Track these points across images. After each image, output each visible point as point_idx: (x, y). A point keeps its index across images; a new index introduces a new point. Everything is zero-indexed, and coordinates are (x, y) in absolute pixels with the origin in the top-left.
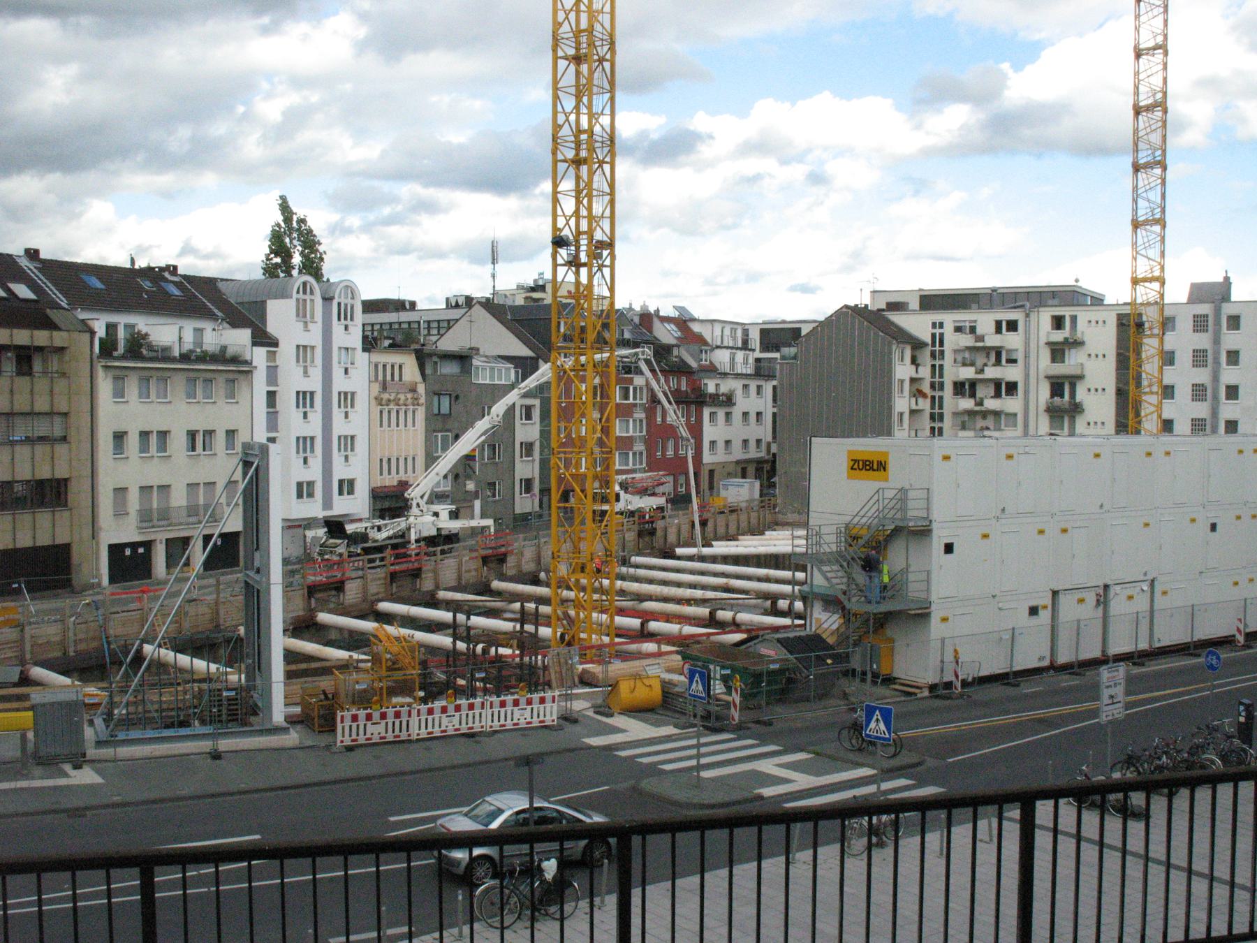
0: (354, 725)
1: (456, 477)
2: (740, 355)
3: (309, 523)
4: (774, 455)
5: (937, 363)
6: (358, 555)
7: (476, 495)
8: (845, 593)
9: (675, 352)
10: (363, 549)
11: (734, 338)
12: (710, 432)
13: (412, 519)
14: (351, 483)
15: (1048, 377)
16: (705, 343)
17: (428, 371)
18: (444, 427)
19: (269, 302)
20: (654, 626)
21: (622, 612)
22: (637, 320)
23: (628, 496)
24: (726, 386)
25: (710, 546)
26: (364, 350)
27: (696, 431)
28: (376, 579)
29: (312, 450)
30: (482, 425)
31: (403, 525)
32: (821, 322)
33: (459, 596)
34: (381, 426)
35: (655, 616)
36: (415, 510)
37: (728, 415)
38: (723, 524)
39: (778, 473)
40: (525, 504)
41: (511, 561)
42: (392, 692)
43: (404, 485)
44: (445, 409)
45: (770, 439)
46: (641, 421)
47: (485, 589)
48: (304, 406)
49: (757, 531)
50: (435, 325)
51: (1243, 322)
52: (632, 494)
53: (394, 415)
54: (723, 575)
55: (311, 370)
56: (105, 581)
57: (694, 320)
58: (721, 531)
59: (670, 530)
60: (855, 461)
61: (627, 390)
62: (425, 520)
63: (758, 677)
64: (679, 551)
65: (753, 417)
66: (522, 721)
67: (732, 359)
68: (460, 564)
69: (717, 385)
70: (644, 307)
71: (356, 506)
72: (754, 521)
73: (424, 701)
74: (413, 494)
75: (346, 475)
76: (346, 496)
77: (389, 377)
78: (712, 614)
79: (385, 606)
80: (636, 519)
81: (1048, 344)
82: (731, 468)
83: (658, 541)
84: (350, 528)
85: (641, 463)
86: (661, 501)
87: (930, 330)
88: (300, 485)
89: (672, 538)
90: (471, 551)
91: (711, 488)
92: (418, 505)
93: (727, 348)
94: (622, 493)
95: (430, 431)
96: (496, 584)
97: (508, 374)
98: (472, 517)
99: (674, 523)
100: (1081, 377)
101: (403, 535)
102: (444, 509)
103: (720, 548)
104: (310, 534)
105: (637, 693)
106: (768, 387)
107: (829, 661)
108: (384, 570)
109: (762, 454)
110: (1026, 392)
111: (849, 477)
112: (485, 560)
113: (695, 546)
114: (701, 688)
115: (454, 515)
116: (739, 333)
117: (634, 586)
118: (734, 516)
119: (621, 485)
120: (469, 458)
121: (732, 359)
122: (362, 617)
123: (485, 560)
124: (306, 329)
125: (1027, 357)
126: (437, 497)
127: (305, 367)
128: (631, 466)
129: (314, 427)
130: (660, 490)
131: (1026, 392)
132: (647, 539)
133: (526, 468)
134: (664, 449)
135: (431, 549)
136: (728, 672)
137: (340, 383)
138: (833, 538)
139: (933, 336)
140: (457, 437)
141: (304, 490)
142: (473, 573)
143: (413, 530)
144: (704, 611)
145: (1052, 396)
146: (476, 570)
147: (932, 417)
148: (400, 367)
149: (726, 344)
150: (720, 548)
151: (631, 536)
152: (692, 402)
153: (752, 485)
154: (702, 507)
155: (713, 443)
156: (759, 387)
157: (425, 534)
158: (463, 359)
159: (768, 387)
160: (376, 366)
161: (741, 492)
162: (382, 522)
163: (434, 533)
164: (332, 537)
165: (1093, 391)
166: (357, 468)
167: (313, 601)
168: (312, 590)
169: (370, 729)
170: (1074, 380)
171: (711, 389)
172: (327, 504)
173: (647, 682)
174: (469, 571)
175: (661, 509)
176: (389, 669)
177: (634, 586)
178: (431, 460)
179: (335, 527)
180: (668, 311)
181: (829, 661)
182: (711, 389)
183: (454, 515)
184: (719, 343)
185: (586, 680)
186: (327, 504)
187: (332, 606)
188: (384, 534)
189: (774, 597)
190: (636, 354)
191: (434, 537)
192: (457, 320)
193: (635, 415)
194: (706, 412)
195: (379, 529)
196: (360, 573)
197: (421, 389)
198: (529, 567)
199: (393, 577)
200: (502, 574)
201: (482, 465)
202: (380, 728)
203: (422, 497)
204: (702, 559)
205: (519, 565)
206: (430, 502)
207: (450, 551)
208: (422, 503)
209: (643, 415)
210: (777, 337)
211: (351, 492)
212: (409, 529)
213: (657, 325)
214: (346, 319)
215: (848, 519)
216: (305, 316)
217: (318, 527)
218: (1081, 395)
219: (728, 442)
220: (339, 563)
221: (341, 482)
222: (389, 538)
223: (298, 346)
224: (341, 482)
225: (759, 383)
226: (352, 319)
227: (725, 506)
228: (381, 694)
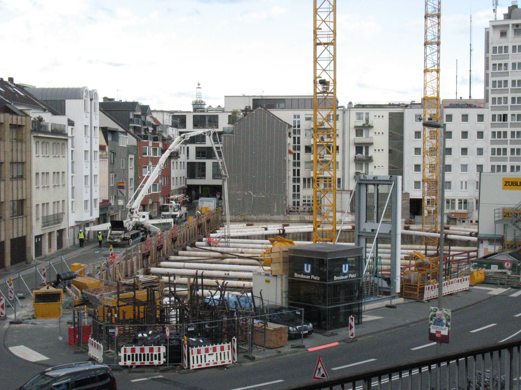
0: (222, 353)
5: (297, 136)
15: (355, 144)
19: (67, 101)
51: (453, 117)
56: (34, 257)
60: (507, 182)
66: (211, 362)
81: (355, 127)
87: (293, 119)
100: (372, 144)
110: (343, 151)
111: (503, 189)
125: (344, 133)
131: (343, 151)
139: (295, 122)
145: (356, 154)
147: (294, 164)
165: (377, 150)
169: (209, 358)
170: (368, 145)
202: (213, 357)
218: (371, 153)
219: (177, 178)
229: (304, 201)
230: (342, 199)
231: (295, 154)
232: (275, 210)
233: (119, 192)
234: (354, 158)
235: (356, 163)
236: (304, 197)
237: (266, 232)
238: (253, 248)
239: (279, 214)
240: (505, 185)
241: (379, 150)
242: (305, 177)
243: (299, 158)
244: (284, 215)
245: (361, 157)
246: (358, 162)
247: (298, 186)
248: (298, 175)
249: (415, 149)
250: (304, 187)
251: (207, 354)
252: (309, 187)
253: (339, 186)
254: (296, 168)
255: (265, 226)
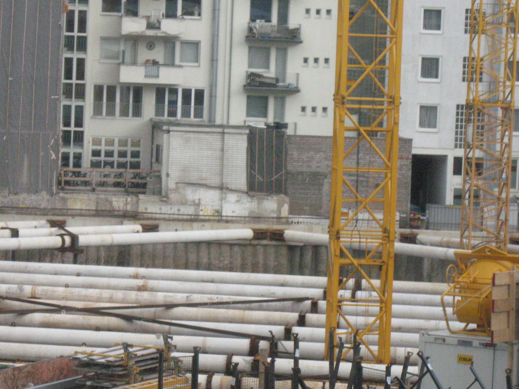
145: (253, 19)
229: (96, 153)
230: (222, 150)
231: (73, 12)
232: (24, 178)
234: (245, 33)
235: (250, 48)
236: (97, 141)
237: (12, 243)
238: (67, 286)
239: (36, 192)
241: (318, 12)
242: (99, 82)
243: (83, 27)
244: (52, 195)
245: (269, 30)
246: (258, 43)
247: (80, 110)
248: (81, 75)
249: (426, 11)
250: (97, 111)
252: (111, 112)
253: (199, 114)
254: (75, 56)
255: (13, 225)
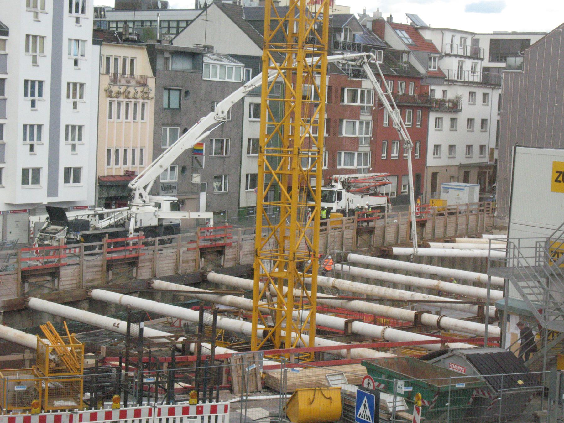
0: (213, 416)
1: (183, 169)
2: (468, 64)
3: (33, 209)
4: (496, 160)
6: (78, 242)
7: (202, 188)
8: (540, 311)
9: (405, 58)
10: (82, 236)
11: (464, 47)
12: (434, 137)
13: (134, 209)
14: (37, 171)
16: (435, 51)
17: (160, 65)
18: (173, 120)
20: (358, 326)
21: (324, 309)
22: (369, 26)
23: (349, 195)
24: (452, 93)
25: (428, 246)
26: (95, 43)
27: (420, 136)
28: (92, 265)
29: (39, 138)
30: (208, 120)
31: (125, 214)
32: (546, 34)
33: (174, 286)
34: (110, 117)
35: (361, 316)
36: (137, 200)
37: (453, 120)
38: (442, 225)
39: (498, 180)
40: (249, 198)
41: (229, 253)
42: (56, 393)
43: (130, 175)
44: (174, 104)
45: (493, 145)
46: (368, 123)
47: (200, 280)
48: (33, 94)
49: (475, 234)
50: (175, 24)
52: (354, 193)
53: (131, 107)
54: (433, 276)
55: (39, 60)
57: (426, 28)
58: (439, 232)
59: (388, 230)
61: (355, 92)
62: (146, 211)
63: (443, 395)
64: (397, 250)
65: (477, 124)
67: (460, 67)
68: (178, 254)
69: (444, 92)
70: (377, 13)
71: (81, 195)
72: (472, 224)
73: (92, 404)
74: (136, 184)
75: (73, 164)
76: (71, 184)
77: (120, 71)
78: (418, 316)
79: (99, 293)
80: (356, 217)
82: (454, 173)
83: (376, 240)
84: (71, 215)
85: (366, 164)
86: (381, 201)
88: (25, 172)
89: (390, 237)
90: (192, 242)
91: (434, 188)
92: (141, 195)
93: (456, 56)
94: (344, 192)
95: (159, 124)
96: (213, 276)
97: (238, 72)
98: (198, 210)
99: (391, 224)
101: (123, 224)
102: (166, 201)
103: (437, 249)
104: (34, 219)
105: (316, 405)
106: (494, 95)
107: (520, 382)
108: (99, 258)
109: (485, 160)
111: (554, 190)
112: (203, 252)
113: (411, 246)
114: (368, 413)
115: (175, 207)
116: (469, 43)
117: (346, 284)
118: (452, 219)
119: (344, 184)
120: (196, 151)
121: (460, 67)
122: (74, 304)
123: (203, 252)
124: (36, 18)
126: (159, 188)
127: (35, 57)
128: (355, 166)
129: (42, 115)
130: (383, 190)
132: (365, 237)
133: (250, 165)
134: (389, 152)
135: (150, 239)
136: (410, 389)
137: (69, 74)
138: (532, 252)
140: (185, 130)
141: (30, 176)
142: (192, 264)
143: (133, 221)
144: (409, 313)
146: (194, 261)
148: (132, 61)
149: (455, 52)
150: (437, 249)
151: (349, 234)
152: (419, 108)
153: (472, 189)
154: (422, 209)
155: (437, 147)
156: (485, 95)
157: (146, 224)
158: (194, 56)
159: (494, 95)
160: (108, 59)
161: (462, 195)
162: (105, 211)
163: (155, 223)
164: (53, 224)
166: (85, 157)
167: (26, 285)
168: (26, 275)
171: (438, 95)
172: (53, 190)
173: (326, 393)
174: (187, 262)
175: (382, 209)
176: (52, 371)
177: (346, 284)
178: (158, 151)
179: (56, 213)
180: (400, 19)
181: (520, 382)
182: (438, 95)
183: (175, 207)
184: (448, 51)
185: (269, 386)
186: (53, 190)
187: (46, 291)
188: (105, 223)
189: (481, 303)
190: (362, 57)
191: (155, 227)
192: (192, 21)
193: (362, 118)
194: (432, 117)
195: (101, 217)
196: (76, 260)
197: (151, 83)
198: (245, 260)
199: (110, 265)
200: (220, 266)
201: (209, 159)
203: (145, 188)
204: (419, 259)
205: (236, 258)
206: (151, 193)
207: (171, 241)
208: (145, 194)
209: (370, 118)
210: (502, 47)
211: (77, 180)
212: (129, 219)
213: (389, 30)
214: (77, 11)
215: (550, 233)
216: (35, 7)
217: (41, 213)
219: (452, 147)
220: (57, 249)
221: (67, 170)
222: (110, 226)
223: (28, 36)
224: (67, 170)
225: (486, 91)
226: (83, 12)
227: (444, 209)
228: (43, 395)
233: (194, 160)
240: (556, 181)
251: (185, 417)
